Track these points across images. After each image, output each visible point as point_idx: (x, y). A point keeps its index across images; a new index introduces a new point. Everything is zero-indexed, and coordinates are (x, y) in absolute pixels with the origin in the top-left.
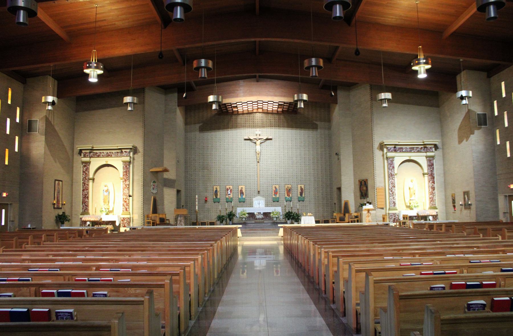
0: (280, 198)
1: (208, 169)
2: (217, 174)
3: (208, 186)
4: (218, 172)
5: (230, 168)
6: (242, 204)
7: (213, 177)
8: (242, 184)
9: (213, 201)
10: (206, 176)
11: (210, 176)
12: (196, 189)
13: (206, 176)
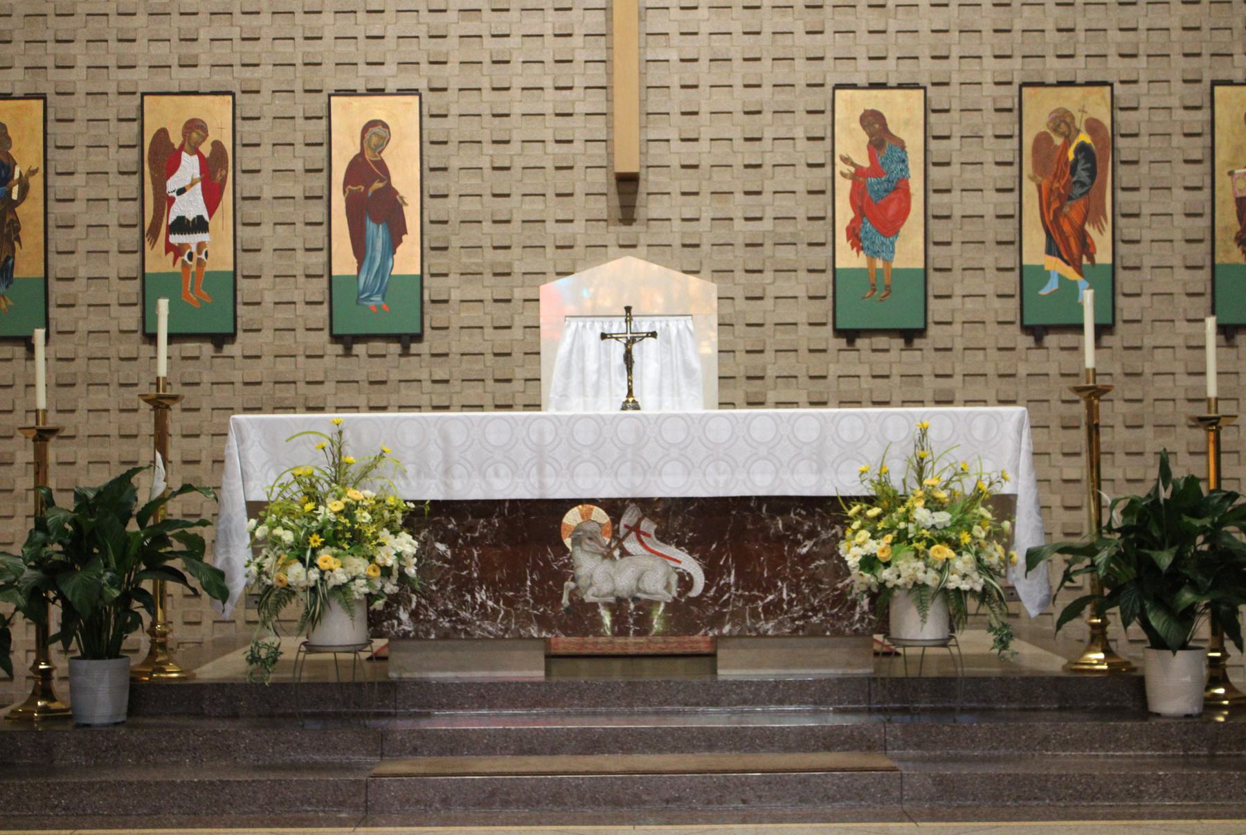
6: (378, 369)
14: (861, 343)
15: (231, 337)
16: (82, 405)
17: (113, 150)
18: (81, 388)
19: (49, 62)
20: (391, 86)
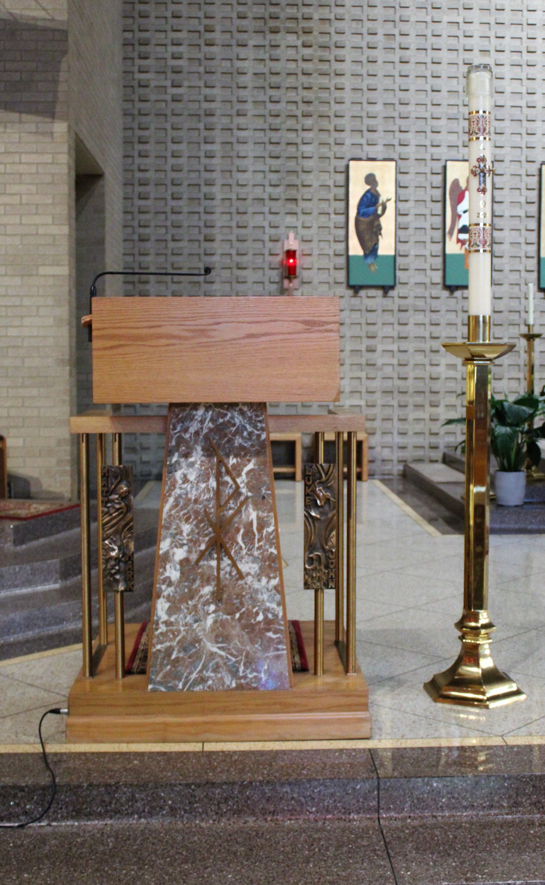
0: (400, 261)
1: (308, 32)
2: (380, 69)
3: (308, 164)
4: (379, 55)
5: (476, 29)
6: (371, 303)
7: (347, 95)
8: (372, 151)
9: (341, 276)
10: (291, 81)
11: (324, 81)
12: (210, 183)
13: (291, 81)
14: (363, 293)
15: (392, 287)
16: (412, 321)
17: (429, 188)
18: (411, 312)
19: (396, 142)
20: (380, 157)
